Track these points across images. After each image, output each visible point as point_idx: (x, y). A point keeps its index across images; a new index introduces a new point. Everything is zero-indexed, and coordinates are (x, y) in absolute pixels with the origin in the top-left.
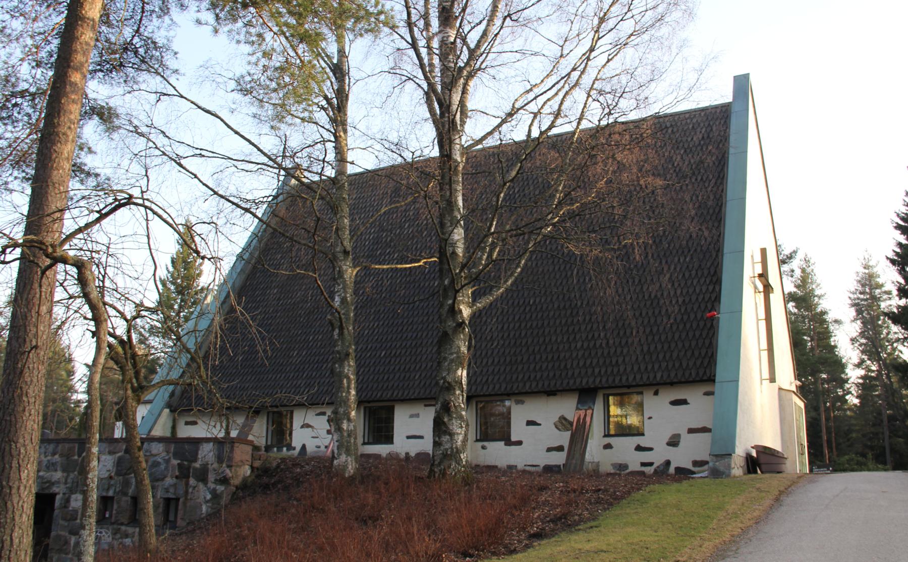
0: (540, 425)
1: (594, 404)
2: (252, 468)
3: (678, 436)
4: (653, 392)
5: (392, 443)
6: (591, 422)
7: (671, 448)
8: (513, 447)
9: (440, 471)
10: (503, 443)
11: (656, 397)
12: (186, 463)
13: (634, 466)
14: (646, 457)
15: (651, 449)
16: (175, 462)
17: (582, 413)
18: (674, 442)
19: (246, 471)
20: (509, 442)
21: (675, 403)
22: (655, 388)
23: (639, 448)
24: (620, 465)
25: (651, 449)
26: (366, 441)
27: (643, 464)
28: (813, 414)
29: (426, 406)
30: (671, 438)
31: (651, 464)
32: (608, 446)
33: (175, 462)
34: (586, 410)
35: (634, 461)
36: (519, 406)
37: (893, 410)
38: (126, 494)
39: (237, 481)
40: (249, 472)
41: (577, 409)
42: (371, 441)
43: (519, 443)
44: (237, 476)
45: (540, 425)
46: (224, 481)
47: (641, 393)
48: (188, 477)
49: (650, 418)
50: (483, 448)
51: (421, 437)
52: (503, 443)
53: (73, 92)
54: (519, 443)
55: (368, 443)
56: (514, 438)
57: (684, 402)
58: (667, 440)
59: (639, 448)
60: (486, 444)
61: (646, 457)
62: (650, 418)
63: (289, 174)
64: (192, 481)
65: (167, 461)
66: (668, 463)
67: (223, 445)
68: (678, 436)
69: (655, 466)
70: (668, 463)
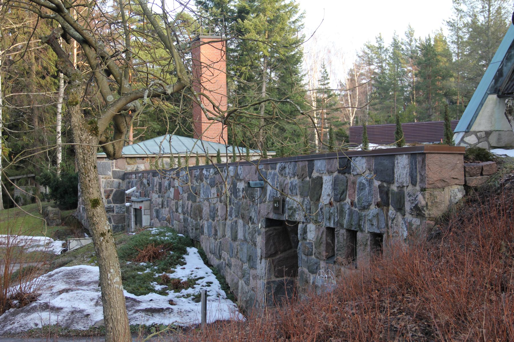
2: (466, 187)
9: (122, 226)
12: (385, 185)
16: (377, 183)
19: (456, 193)
28: (222, 280)
33: (377, 183)
37: (413, 111)
38: (342, 226)
39: (436, 212)
40: (460, 195)
44: (435, 203)
46: (418, 211)
48: (388, 205)
51: (98, 158)
53: (56, 203)
63: (335, 262)
64: (392, 211)
65: (370, 182)
67: (367, 109)
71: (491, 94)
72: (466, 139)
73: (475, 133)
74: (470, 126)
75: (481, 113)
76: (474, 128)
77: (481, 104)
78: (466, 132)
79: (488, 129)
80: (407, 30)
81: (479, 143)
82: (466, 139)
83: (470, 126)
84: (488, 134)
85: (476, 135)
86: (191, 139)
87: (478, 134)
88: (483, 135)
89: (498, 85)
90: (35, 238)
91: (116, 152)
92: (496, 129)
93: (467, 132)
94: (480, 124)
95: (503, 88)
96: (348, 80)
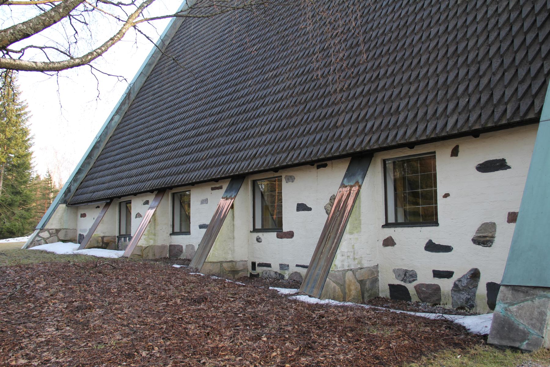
0: (310, 209)
1: (363, 178)
3: (492, 226)
4: (449, 151)
5: (436, 224)
6: (353, 206)
7: (480, 247)
8: (285, 240)
10: (275, 234)
11: (454, 158)
13: (425, 278)
14: (441, 261)
15: (447, 249)
17: (345, 191)
18: (484, 239)
20: (282, 235)
21: (487, 167)
22: (452, 144)
23: (431, 247)
24: (406, 272)
25: (447, 249)
26: (391, 220)
27: (438, 274)
29: (213, 189)
30: (479, 231)
31: (448, 275)
32: (389, 242)
34: (351, 187)
35: (425, 266)
36: (290, 183)
41: (343, 185)
42: (401, 220)
43: (290, 235)
45: (310, 209)
47: (190, 191)
49: (446, 196)
50: (258, 240)
52: (275, 234)
54: (290, 235)
55: (396, 225)
56: (285, 229)
57: (499, 165)
58: (472, 234)
59: (431, 247)
60: (260, 235)
61: (441, 261)
62: (446, 196)
66: (475, 275)
68: (492, 226)
69: (455, 278)
70: (475, 275)
71: (61, 203)
72: (41, 234)
73: (48, 230)
74: (44, 225)
75: (53, 216)
76: (47, 227)
77: (54, 210)
78: (41, 229)
79: (58, 228)
80: (509, 163)
81: (50, 237)
82: (41, 234)
83: (44, 225)
84: (58, 231)
85: (49, 232)
86: (49, 28)
87: (50, 231)
88: (54, 231)
89: (67, 198)
90: (276, 288)
91: (519, 355)
92: (64, 228)
93: (42, 229)
94: (52, 224)
95: (69, 201)
96: (455, 153)
